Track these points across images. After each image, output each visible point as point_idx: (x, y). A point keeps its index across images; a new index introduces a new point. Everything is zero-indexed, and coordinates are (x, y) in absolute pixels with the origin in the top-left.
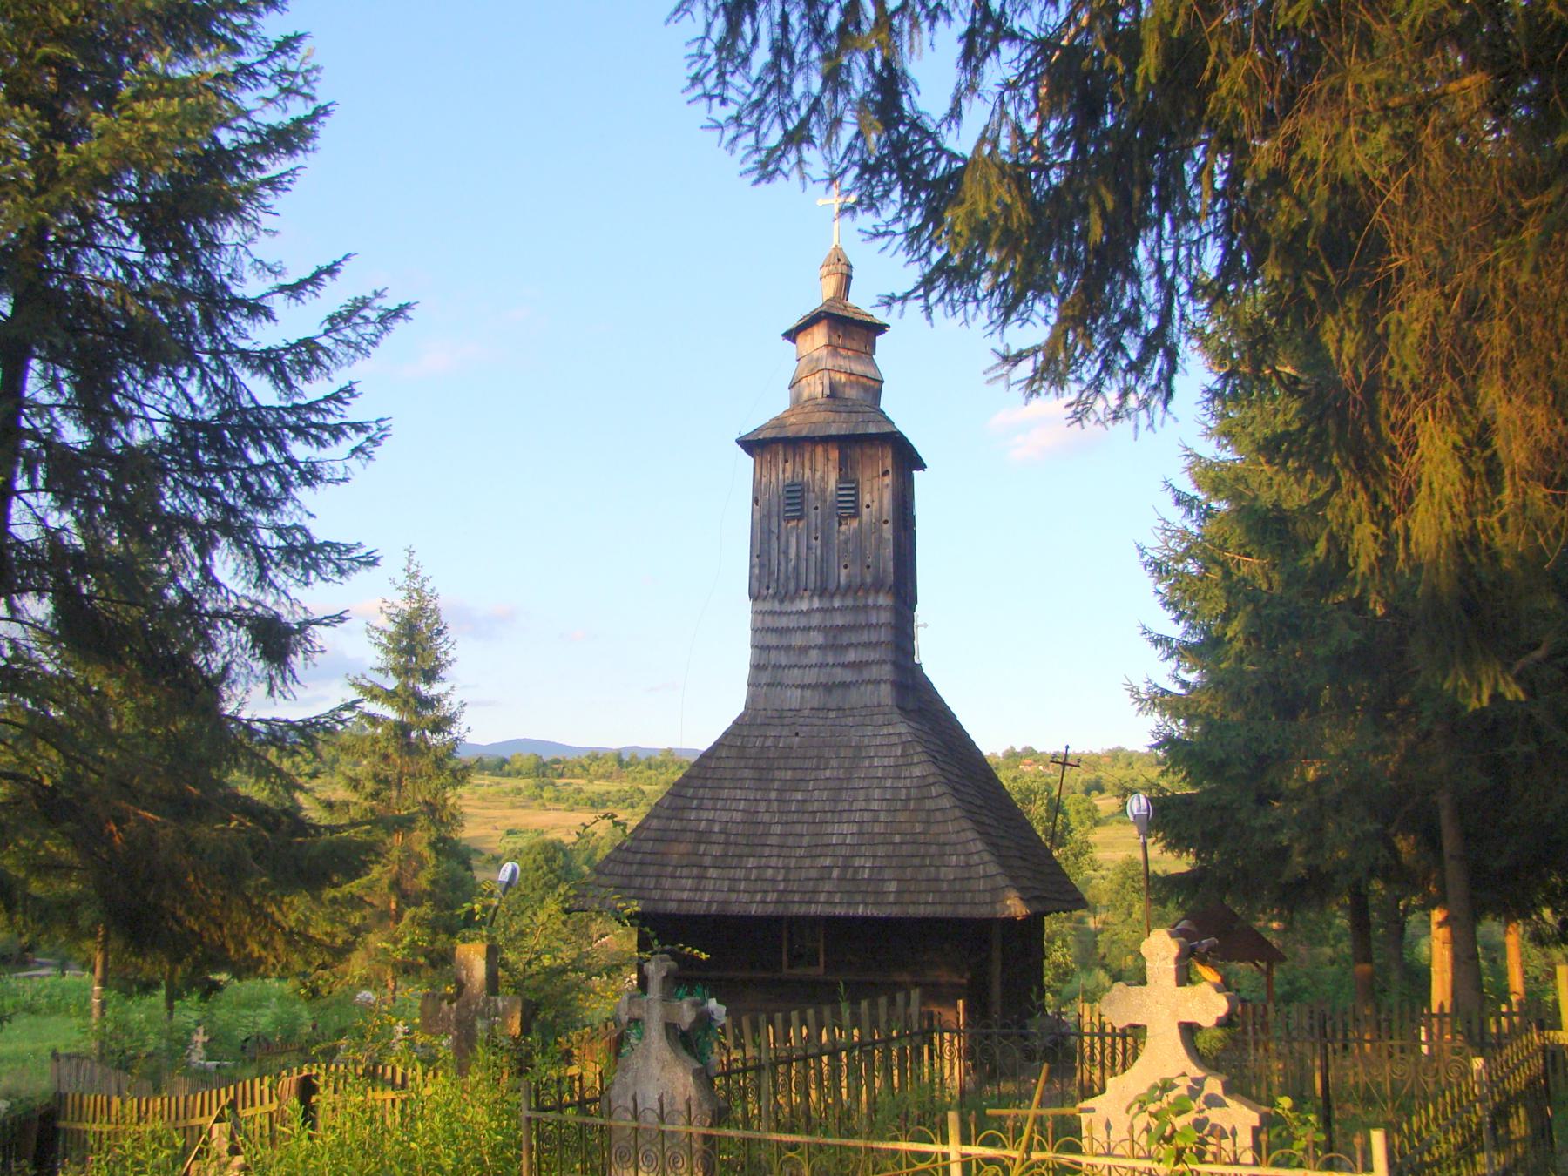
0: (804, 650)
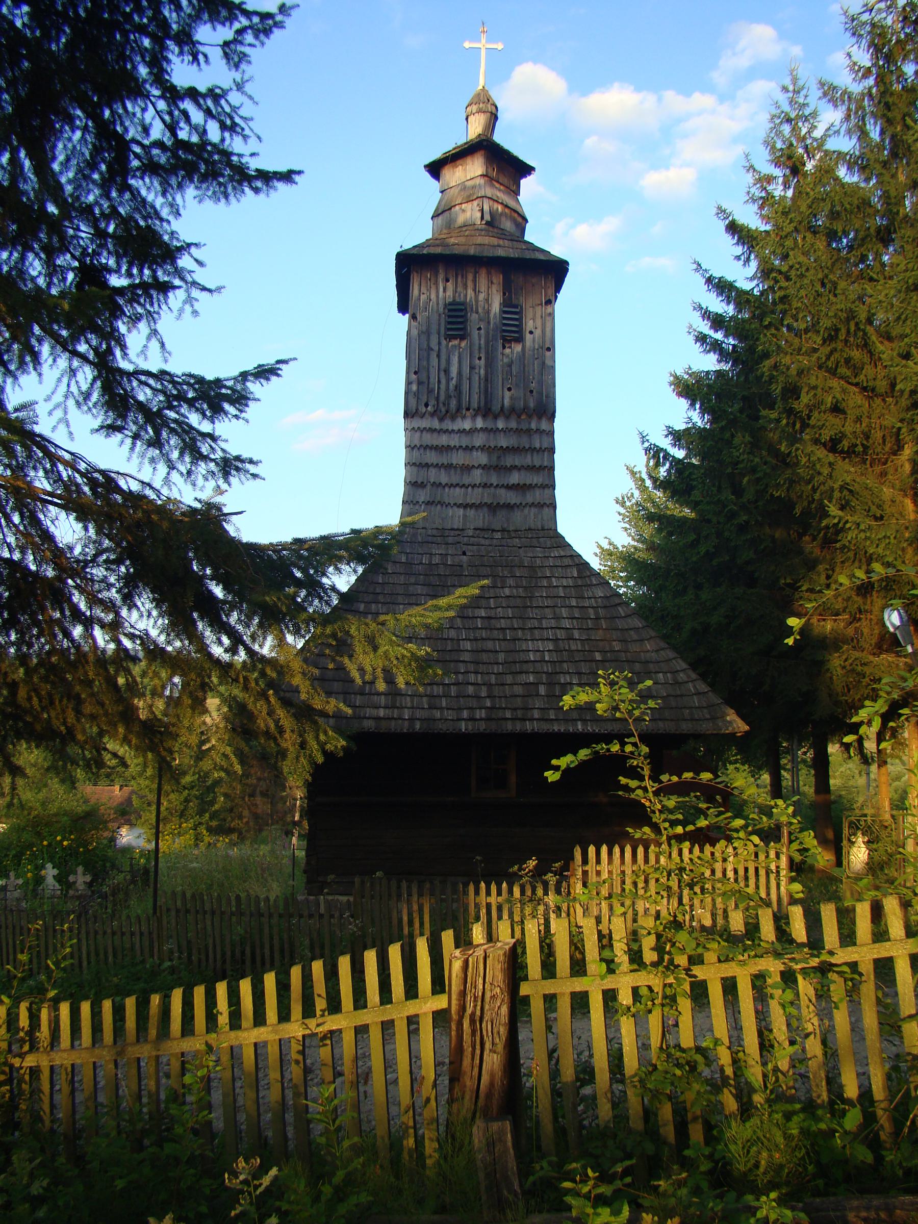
0: (467, 469)
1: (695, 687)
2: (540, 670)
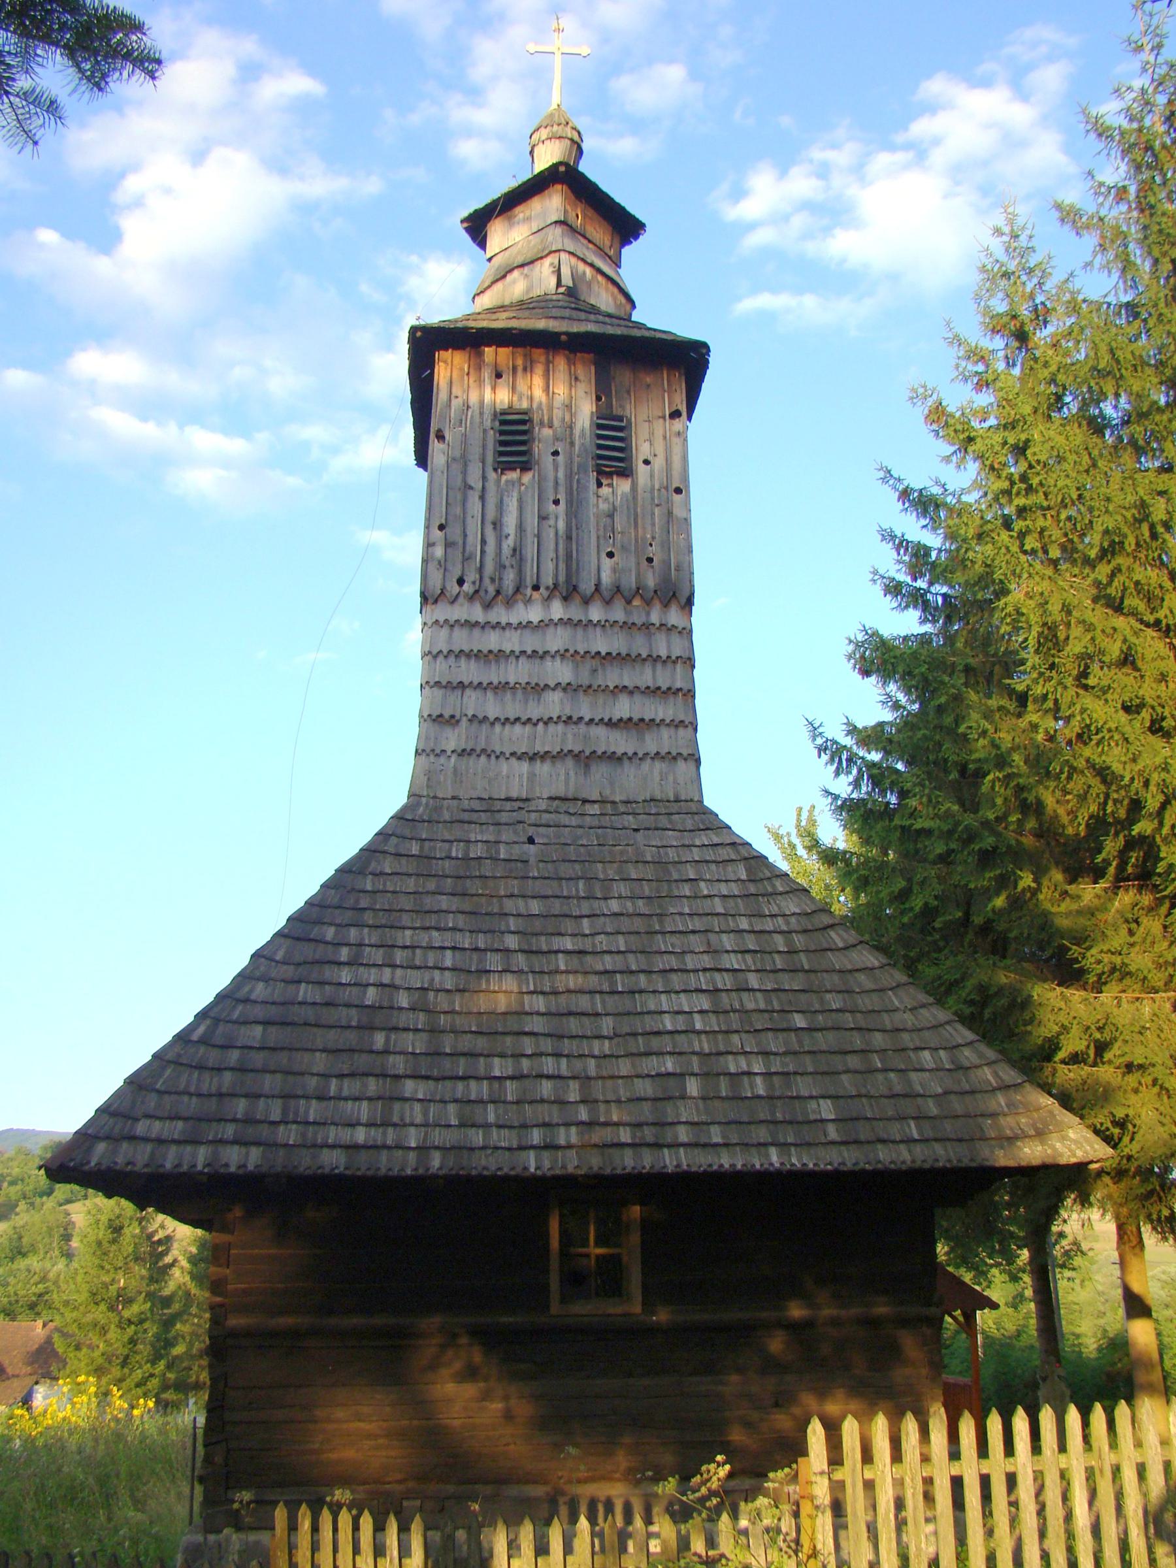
0: (537, 689)
1: (996, 1074)
2: (686, 1048)
